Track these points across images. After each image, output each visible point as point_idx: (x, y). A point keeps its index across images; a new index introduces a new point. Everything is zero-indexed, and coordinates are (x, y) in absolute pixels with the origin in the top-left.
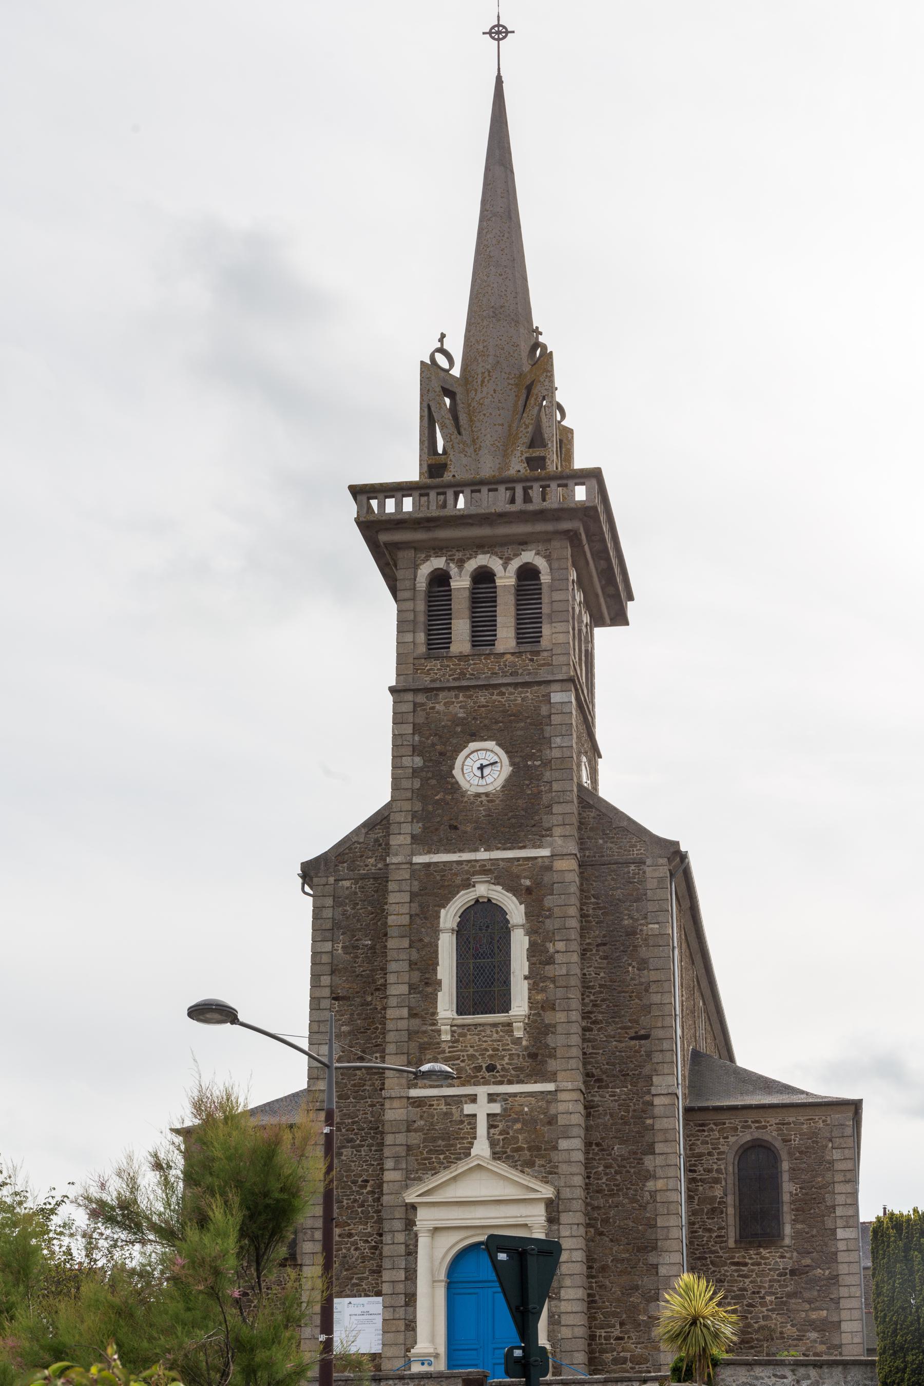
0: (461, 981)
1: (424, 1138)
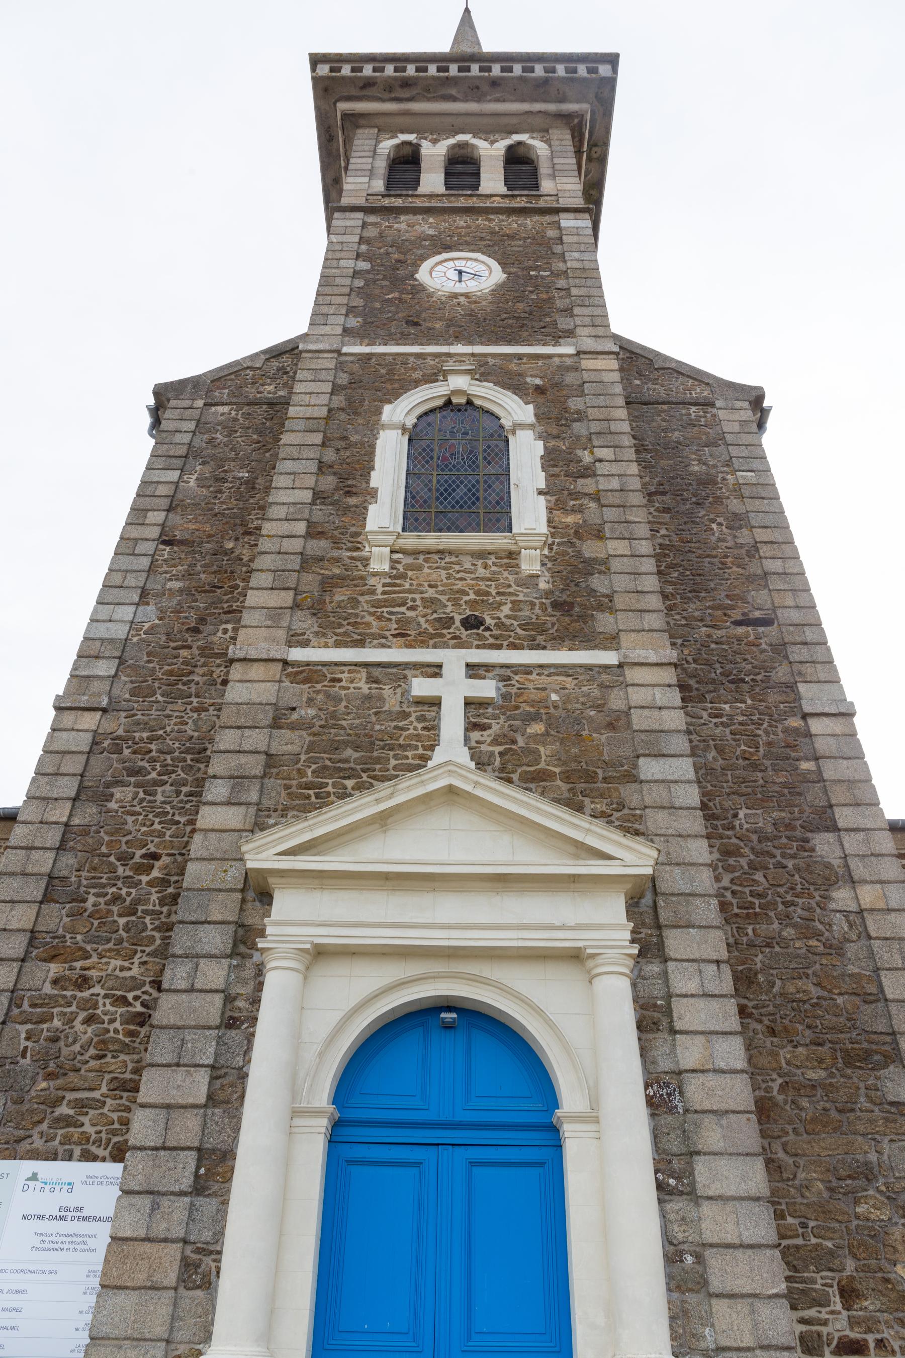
0: (413, 497)
1: (312, 743)
